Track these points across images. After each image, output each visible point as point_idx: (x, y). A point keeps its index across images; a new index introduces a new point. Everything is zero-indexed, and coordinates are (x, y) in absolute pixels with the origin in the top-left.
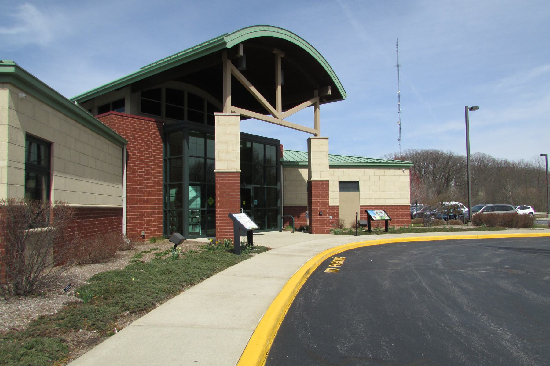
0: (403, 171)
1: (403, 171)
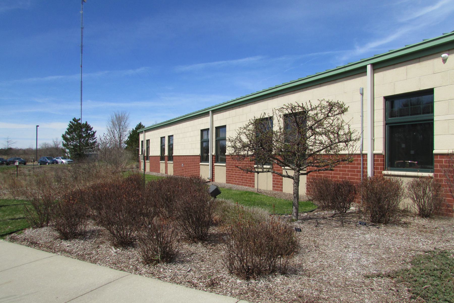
0: (444, 60)
1: (444, 60)
